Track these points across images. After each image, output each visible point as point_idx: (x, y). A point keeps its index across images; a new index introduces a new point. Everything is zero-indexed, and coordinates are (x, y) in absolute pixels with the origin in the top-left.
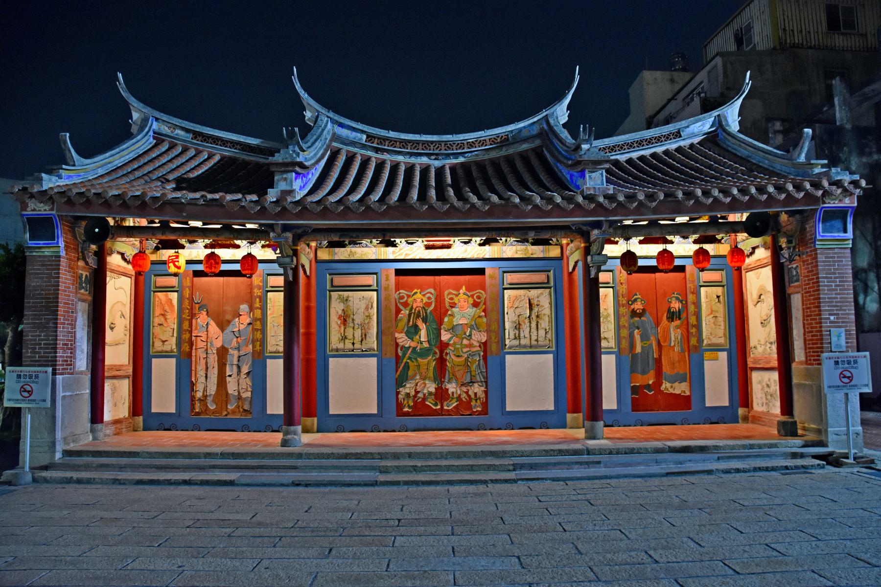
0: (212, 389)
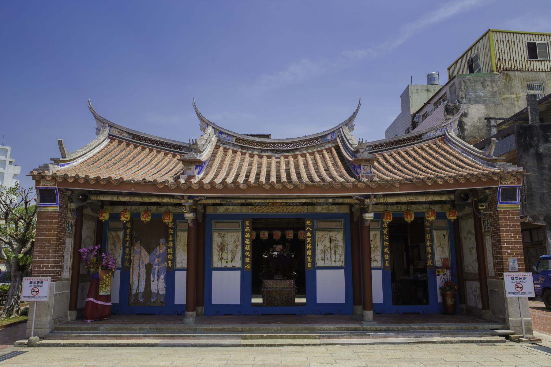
0: (142, 289)
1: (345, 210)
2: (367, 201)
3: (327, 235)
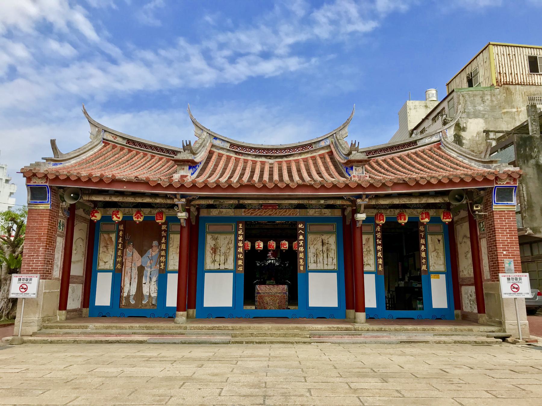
0: (133, 291)
1: (337, 213)
2: (359, 201)
3: (319, 238)
